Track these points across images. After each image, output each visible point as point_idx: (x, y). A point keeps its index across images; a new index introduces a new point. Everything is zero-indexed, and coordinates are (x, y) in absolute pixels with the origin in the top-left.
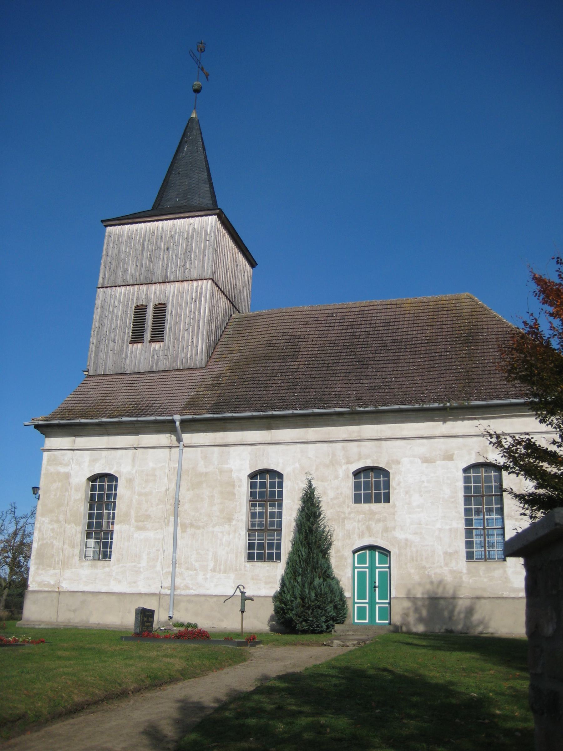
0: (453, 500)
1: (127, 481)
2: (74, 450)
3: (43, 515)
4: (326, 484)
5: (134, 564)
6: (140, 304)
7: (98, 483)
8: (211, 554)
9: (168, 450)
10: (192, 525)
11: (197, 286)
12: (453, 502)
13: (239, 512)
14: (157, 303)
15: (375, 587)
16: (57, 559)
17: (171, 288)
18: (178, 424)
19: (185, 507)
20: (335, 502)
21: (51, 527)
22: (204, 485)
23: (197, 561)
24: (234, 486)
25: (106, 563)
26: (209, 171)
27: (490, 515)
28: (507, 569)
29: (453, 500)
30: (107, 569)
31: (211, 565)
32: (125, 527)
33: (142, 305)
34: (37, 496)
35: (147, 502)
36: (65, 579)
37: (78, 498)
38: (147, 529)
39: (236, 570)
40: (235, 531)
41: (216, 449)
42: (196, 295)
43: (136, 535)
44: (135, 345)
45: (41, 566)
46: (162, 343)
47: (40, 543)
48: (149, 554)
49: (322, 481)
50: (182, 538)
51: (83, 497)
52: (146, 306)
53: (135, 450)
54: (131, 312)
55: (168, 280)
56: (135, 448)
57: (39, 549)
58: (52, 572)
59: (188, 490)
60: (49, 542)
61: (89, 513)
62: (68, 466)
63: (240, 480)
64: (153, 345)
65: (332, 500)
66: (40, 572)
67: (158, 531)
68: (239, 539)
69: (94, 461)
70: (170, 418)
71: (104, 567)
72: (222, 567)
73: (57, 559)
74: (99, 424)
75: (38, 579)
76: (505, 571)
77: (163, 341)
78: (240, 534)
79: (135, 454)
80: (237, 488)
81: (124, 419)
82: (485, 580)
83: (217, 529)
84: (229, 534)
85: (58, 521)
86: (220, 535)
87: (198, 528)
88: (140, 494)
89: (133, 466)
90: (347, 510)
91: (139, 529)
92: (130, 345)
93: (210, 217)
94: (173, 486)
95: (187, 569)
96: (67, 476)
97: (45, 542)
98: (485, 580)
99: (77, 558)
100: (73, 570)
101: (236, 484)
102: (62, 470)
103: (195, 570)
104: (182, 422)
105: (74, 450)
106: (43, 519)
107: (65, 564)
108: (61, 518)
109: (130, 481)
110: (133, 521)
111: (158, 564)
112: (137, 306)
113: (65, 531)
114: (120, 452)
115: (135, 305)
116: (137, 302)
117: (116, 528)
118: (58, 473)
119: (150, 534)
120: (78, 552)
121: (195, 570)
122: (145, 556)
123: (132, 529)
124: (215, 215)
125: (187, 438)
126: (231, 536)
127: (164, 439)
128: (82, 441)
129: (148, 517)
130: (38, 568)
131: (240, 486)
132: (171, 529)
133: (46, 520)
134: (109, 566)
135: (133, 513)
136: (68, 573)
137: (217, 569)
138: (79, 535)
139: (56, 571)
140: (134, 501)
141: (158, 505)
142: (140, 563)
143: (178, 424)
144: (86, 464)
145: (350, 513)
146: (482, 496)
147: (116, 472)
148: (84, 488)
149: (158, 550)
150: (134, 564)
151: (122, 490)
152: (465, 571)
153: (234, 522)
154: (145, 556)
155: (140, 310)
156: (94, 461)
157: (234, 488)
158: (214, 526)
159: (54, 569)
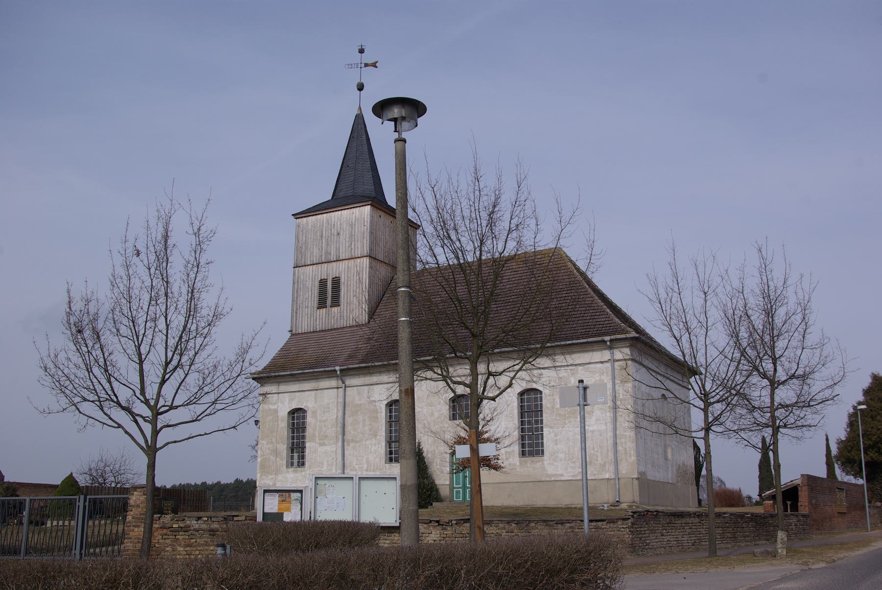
0: (511, 415)
1: (312, 413)
2: (279, 393)
3: (262, 439)
4: (433, 408)
5: (319, 469)
6: (322, 278)
7: (526, 397)
8: (365, 459)
9: (336, 390)
10: (353, 440)
11: (360, 262)
12: (511, 417)
13: (381, 430)
14: (334, 277)
15: (466, 477)
16: (273, 468)
17: (342, 265)
18: (338, 372)
19: (348, 428)
20: (439, 420)
21: (268, 447)
22: (359, 413)
23: (357, 465)
24: (377, 412)
25: (302, 469)
26: (144, 434)
27: (537, 425)
28: (544, 462)
29: (511, 415)
30: (303, 473)
31: (365, 466)
32: (313, 444)
33: (324, 279)
34: (258, 426)
35: (325, 426)
36: (278, 482)
37: (283, 426)
38: (326, 445)
39: (380, 470)
40: (379, 444)
41: (366, 387)
42: (360, 269)
43: (319, 449)
44: (321, 310)
45: (264, 474)
46: (339, 308)
47: (262, 458)
48: (328, 461)
49: (431, 406)
50: (347, 449)
51: (286, 425)
52: (327, 279)
53: (316, 391)
54: (317, 284)
55: (341, 259)
56: (316, 390)
57: (261, 462)
58: (270, 477)
59: (350, 417)
60: (267, 457)
61: (522, 450)
62: (275, 404)
63: (381, 408)
64: (333, 309)
65: (436, 419)
66: (263, 477)
67: (333, 445)
68: (382, 448)
69: (291, 400)
70: (333, 369)
71: (301, 472)
72: (372, 468)
73: (273, 468)
74: (291, 375)
75: (263, 482)
76: (543, 464)
77: (339, 306)
78: (382, 445)
79: (316, 393)
80: (379, 414)
81: (306, 371)
82: (531, 470)
83: (368, 442)
84: (375, 445)
85: (272, 443)
86: (370, 446)
87: (356, 442)
88: (321, 421)
89: (316, 402)
90: (446, 425)
91: (322, 445)
92: (318, 310)
93: (366, 207)
94: (340, 414)
95: (351, 470)
96: (276, 411)
97: (265, 457)
98: (531, 470)
99: (285, 467)
100: (283, 475)
101: (378, 411)
102: (272, 407)
103: (356, 470)
104: (341, 370)
105: (279, 393)
106: (263, 442)
107: (277, 472)
108: (274, 440)
109: (314, 412)
110: (317, 439)
111: (334, 468)
112: (321, 280)
113: (276, 449)
114: (307, 393)
115: (319, 279)
116: (321, 277)
117: (307, 445)
118: (270, 409)
119: (328, 448)
120: (285, 462)
121: (356, 470)
122: (325, 463)
123: (317, 445)
124: (369, 205)
125: (350, 381)
126: (377, 446)
127: (333, 383)
128: (283, 387)
129: (327, 436)
130: (261, 475)
131: (381, 413)
132: (340, 444)
133: (264, 442)
134: (304, 471)
135: (317, 433)
136: (280, 477)
137: (369, 470)
138: (285, 451)
139: (273, 476)
140: (317, 426)
141: (332, 428)
142: (322, 468)
143: (338, 372)
144: (287, 402)
145: (448, 427)
146: (533, 411)
147: (305, 406)
148: (286, 419)
149: (333, 459)
150: (319, 469)
151: (309, 419)
152: (518, 464)
153: (378, 437)
154: (325, 463)
155: (323, 283)
156: (291, 400)
157: (377, 414)
158: (366, 441)
159: (272, 475)
